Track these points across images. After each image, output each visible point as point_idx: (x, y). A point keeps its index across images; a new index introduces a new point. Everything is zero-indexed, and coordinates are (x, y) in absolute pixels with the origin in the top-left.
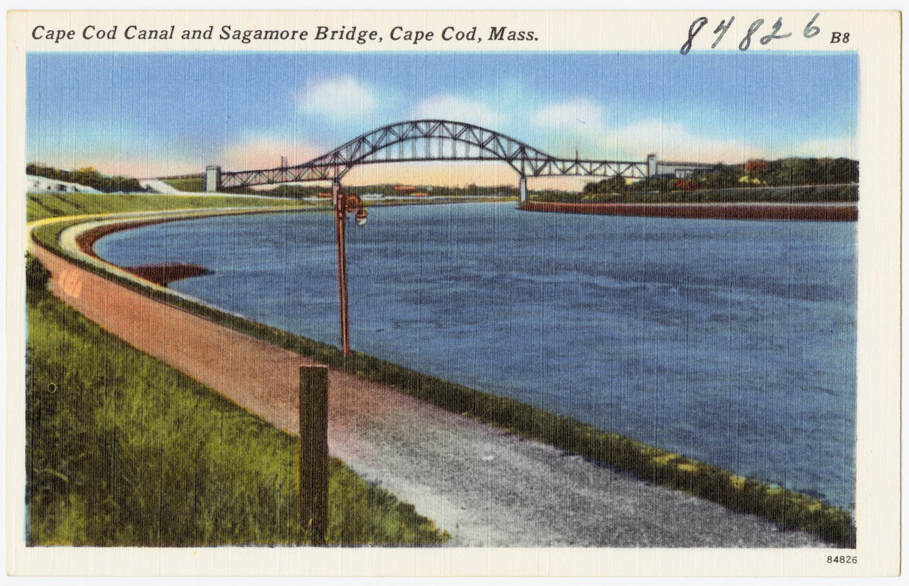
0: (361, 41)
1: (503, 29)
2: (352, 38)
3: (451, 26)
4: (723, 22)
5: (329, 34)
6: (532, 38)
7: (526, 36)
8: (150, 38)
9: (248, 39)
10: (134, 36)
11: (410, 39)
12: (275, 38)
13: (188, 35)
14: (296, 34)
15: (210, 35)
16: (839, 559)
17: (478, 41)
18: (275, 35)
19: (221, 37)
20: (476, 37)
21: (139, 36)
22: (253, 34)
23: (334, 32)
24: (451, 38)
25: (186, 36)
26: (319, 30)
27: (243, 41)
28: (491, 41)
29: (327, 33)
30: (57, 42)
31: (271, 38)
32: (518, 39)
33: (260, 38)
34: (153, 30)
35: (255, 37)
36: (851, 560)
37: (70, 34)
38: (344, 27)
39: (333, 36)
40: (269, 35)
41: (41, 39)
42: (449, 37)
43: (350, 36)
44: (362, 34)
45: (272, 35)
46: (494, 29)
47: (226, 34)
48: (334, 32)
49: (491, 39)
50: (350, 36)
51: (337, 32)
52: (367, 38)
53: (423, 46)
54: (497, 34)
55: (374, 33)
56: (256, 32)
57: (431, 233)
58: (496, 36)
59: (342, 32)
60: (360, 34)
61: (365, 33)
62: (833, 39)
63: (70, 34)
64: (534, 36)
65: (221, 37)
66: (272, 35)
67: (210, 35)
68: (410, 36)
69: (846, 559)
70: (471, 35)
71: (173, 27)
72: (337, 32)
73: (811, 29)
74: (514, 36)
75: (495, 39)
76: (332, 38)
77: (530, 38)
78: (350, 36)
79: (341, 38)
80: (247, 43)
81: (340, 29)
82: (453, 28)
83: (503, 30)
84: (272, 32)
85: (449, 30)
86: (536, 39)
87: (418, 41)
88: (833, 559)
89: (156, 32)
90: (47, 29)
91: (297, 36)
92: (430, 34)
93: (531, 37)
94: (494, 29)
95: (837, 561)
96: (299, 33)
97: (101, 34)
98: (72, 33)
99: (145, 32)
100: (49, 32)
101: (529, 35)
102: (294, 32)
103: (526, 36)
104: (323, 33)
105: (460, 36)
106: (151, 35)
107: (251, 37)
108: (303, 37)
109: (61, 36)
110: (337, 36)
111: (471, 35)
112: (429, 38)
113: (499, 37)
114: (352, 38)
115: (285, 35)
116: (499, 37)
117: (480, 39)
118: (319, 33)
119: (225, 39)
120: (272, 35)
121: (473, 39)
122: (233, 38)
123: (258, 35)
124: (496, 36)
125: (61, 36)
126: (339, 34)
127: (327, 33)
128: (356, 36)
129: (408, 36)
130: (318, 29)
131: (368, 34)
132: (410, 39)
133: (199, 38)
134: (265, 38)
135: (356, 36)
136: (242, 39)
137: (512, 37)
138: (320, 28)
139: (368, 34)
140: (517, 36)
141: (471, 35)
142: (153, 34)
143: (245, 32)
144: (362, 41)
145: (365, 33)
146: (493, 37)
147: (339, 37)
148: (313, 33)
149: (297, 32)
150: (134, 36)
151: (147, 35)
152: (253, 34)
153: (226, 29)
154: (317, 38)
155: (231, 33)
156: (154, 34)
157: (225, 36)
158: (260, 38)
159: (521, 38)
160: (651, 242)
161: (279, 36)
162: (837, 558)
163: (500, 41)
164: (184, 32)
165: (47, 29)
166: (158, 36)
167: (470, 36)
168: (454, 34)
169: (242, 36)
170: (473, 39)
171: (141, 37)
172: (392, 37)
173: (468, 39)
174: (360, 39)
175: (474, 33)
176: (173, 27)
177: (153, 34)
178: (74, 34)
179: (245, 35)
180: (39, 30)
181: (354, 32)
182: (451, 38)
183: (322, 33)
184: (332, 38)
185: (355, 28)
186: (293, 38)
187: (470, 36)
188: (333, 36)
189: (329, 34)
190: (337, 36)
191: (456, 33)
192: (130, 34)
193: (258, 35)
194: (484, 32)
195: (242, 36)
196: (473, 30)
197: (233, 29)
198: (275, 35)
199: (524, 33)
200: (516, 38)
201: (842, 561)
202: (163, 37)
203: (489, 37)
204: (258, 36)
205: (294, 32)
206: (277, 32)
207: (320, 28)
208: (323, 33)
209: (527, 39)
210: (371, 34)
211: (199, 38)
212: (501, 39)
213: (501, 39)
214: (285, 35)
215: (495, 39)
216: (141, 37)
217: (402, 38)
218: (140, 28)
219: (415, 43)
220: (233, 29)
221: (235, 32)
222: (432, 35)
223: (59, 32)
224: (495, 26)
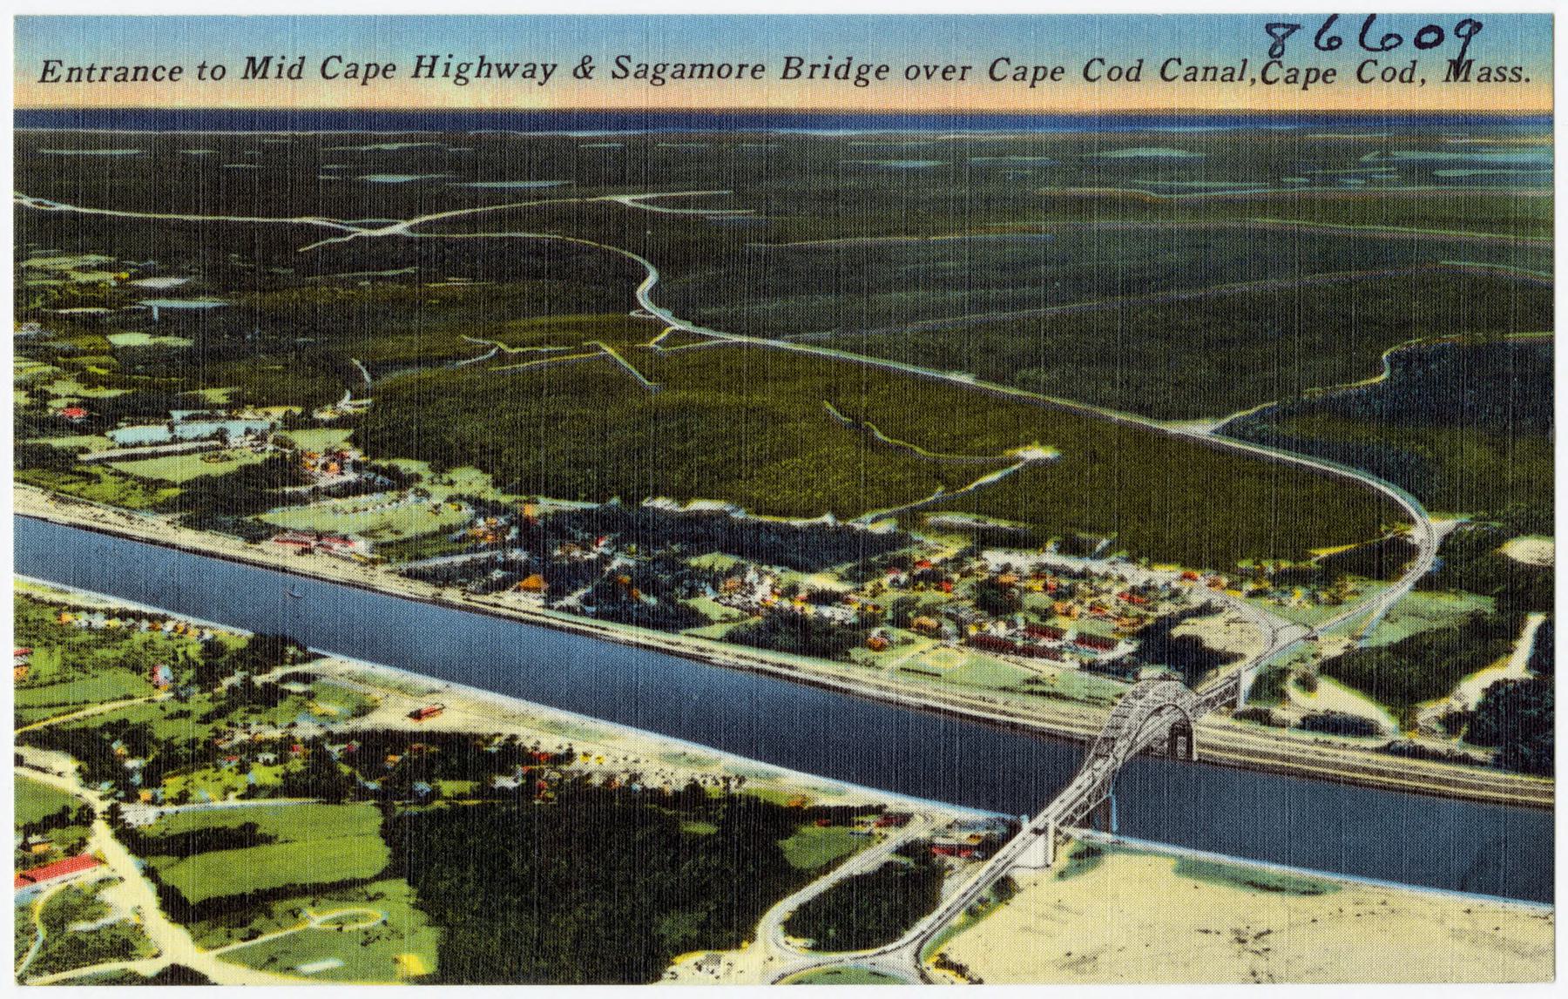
0: (459, 81)
1: (267, 60)
2: (846, 77)
5: (806, 70)
7: (1509, 74)
8: (1204, 79)
13: (125, 75)
14: (745, 69)
15: (847, 72)
19: (614, 76)
20: (1417, 78)
22: (670, 70)
23: (813, 67)
25: (121, 77)
27: (455, 82)
31: (701, 76)
32: (1496, 80)
37: (387, 71)
40: (697, 70)
44: (463, 68)
45: (702, 71)
46: (252, 60)
47: (621, 69)
49: (246, 77)
50: (842, 73)
52: (871, 76)
56: (119, 69)
57: (1387, 180)
58: (255, 73)
59: (828, 67)
60: (859, 69)
64: (1524, 75)
65: (614, 76)
67: (847, 72)
70: (372, 72)
71: (1245, 61)
74: (1489, 74)
75: (254, 77)
77: (1515, 78)
78: (842, 72)
79: (826, 76)
82: (339, 58)
84: (703, 66)
87: (1309, 85)
89: (1216, 69)
91: (747, 72)
92: (390, 68)
94: (252, 60)
96: (750, 69)
97: (1115, 74)
100: (1289, 71)
101: (1498, 71)
103: (1509, 74)
108: (881, 75)
109: (1040, 75)
110: (819, 73)
113: (260, 74)
116: (260, 74)
118: (788, 67)
120: (702, 71)
123: (680, 73)
124: (255, 73)
126: (823, 69)
128: (853, 73)
131: (873, 71)
133: (710, 76)
134: (135, 79)
135: (853, 73)
136: (650, 78)
138: (789, 59)
139: (873, 71)
140: (1494, 74)
141: (372, 72)
142: (1211, 73)
144: (463, 81)
151: (687, 73)
152: (670, 70)
153: (623, 61)
155: (632, 69)
157: (620, 73)
161: (715, 73)
165: (1185, 64)
166: (1218, 77)
169: (651, 72)
171: (1290, 80)
172: (324, 75)
174: (859, 78)
175: (1413, 70)
176: (1245, 61)
177: (1211, 73)
189: (806, 70)
190: (819, 73)
192: (1093, 74)
195: (651, 72)
197: (635, 61)
199: (1505, 69)
200: (1492, 79)
205: (741, 67)
209: (1496, 80)
210: (879, 71)
211: (144, 79)
212: (264, 76)
213: (264, 76)
214: (725, 71)
215: (254, 77)
216: (349, 75)
217: (341, 76)
218: (347, 60)
220: (635, 61)
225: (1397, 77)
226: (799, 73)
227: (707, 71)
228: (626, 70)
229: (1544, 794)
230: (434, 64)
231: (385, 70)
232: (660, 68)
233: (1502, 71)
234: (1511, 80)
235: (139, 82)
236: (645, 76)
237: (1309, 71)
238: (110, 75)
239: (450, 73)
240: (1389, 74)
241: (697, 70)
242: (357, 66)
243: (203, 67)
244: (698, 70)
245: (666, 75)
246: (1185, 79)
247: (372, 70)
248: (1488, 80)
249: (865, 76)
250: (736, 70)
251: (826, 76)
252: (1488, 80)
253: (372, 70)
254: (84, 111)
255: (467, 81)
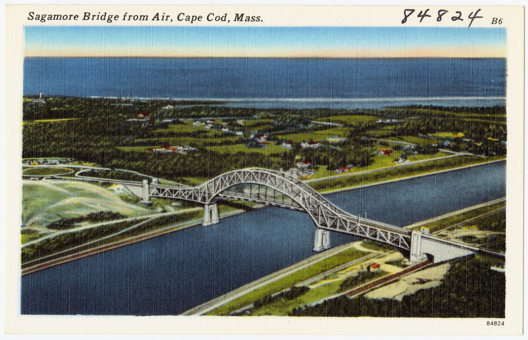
0: (42, 21)
1: (242, 15)
2: (104, 19)
3: (213, 13)
4: (421, 12)
6: (259, 20)
7: (256, 19)
9: (44, 20)
10: (183, 19)
11: (189, 20)
12: (60, 19)
13: (51, 17)
14: (131, 17)
15: (225, 18)
16: (494, 323)
17: (171, 21)
18: (59, 17)
19: (29, 19)
20: (227, 19)
21: (246, 19)
22: (47, 17)
23: (93, 16)
24: (212, 20)
26: (85, 15)
27: (107, 21)
28: (235, 22)
29: (90, 16)
30: (192, 22)
31: (143, 20)
32: (251, 21)
33: (51, 19)
34: (56, 15)
35: (48, 19)
36: (500, 324)
38: (99, 13)
39: (167, 18)
40: (142, 18)
41: (183, 20)
42: (211, 19)
43: (103, 18)
45: (55, 17)
46: (237, 15)
48: (130, 16)
49: (235, 20)
50: (103, 18)
51: (95, 16)
53: (196, 23)
54: (239, 17)
55: (200, 17)
56: (49, 16)
58: (238, 19)
59: (98, 16)
60: (109, 17)
61: (112, 16)
62: (493, 22)
63: (199, 18)
64: (261, 19)
66: (57, 17)
68: (189, 18)
69: (498, 323)
72: (95, 16)
73: (441, 14)
75: (238, 20)
76: (93, 19)
77: (258, 20)
78: (103, 18)
79: (98, 19)
80: (110, 22)
81: (97, 14)
82: (184, 14)
83: (243, 16)
84: (144, 16)
85: (211, 15)
86: (262, 21)
87: (193, 21)
88: (490, 323)
90: (186, 15)
91: (72, 18)
92: (117, 16)
93: (258, 19)
94: (237, 15)
95: (493, 324)
96: (133, 17)
97: (218, 18)
98: (200, 17)
99: (52, 16)
100: (37, 16)
101: (252, 18)
102: (71, 16)
103: (256, 19)
104: (88, 16)
105: (218, 19)
106: (55, 17)
107: (46, 19)
109: (194, 19)
110: (95, 18)
111: (223, 19)
112: (200, 19)
113: (240, 19)
114: (104, 19)
115: (65, 17)
116: (240, 19)
117: (229, 21)
119: (30, 20)
121: (225, 20)
122: (36, 19)
123: (50, 17)
124: (238, 19)
125: (194, 19)
126: (97, 17)
127: (90, 16)
129: (188, 18)
130: (84, 14)
131: (113, 17)
132: (189, 20)
133: (60, 19)
135: (107, 18)
137: (248, 19)
138: (85, 13)
139: (113, 17)
140: (251, 19)
143: (42, 16)
144: (43, 21)
145: (112, 16)
146: (237, 19)
147: (97, 18)
148: (82, 16)
149: (132, 16)
150: (183, 19)
152: (47, 17)
153: (31, 14)
154: (84, 19)
155: (34, 16)
156: (136, 18)
157: (31, 18)
158: (51, 19)
159: (253, 20)
160: (75, 192)
161: (62, 18)
162: (492, 322)
163: (241, 22)
164: (246, 17)
165: (186, 15)
167: (223, 19)
168: (214, 17)
169: (41, 18)
170: (225, 20)
173: (222, 21)
174: (109, 20)
175: (225, 17)
178: (118, 17)
179: (43, 18)
180: (181, 16)
181: (105, 16)
182: (212, 20)
183: (86, 16)
184: (93, 19)
185: (106, 13)
186: (70, 19)
187: (223, 19)
188: (167, 18)
189: (91, 17)
191: (215, 17)
193: (50, 17)
194: (231, 17)
195: (41, 18)
196: (225, 15)
197: (36, 14)
198: (59, 17)
199: (255, 17)
200: (250, 20)
201: (496, 324)
202: (37, 18)
203: (234, 20)
204: (50, 18)
205: (71, 16)
206: (61, 16)
207: (494, 19)
208: (88, 16)
209: (256, 21)
210: (115, 17)
211: (60, 19)
212: (241, 20)
213: (241, 20)
214: (65, 17)
215: (238, 20)
219: (192, 22)
220: (36, 14)
221: (187, 17)
222: (78, 17)
223: (193, 17)
224: (237, 13)
225: (220, 19)
226: (496, 22)
227: (59, 17)
228: (32, 17)
229: (40, 173)
230: (105, 15)
231: (199, 18)
232: (44, 16)
233: (253, 18)
234: (256, 21)
235: (58, 20)
236: (39, 19)
237: (193, 17)
238: (132, 18)
239: (190, 20)
240: (218, 18)
241: (142, 18)
242: (189, 17)
243: (125, 16)
244: (56, 17)
245: (46, 19)
246: (186, 20)
247: (194, 18)
248: (249, 21)
249: (111, 19)
250: (69, 17)
251: (98, 19)
252: (249, 21)
253: (194, 18)
254: (352, 27)
255: (45, 21)
